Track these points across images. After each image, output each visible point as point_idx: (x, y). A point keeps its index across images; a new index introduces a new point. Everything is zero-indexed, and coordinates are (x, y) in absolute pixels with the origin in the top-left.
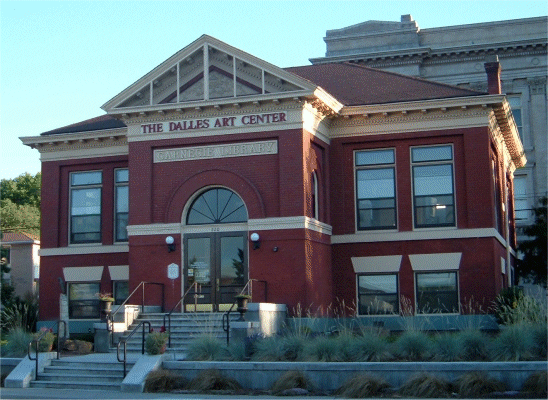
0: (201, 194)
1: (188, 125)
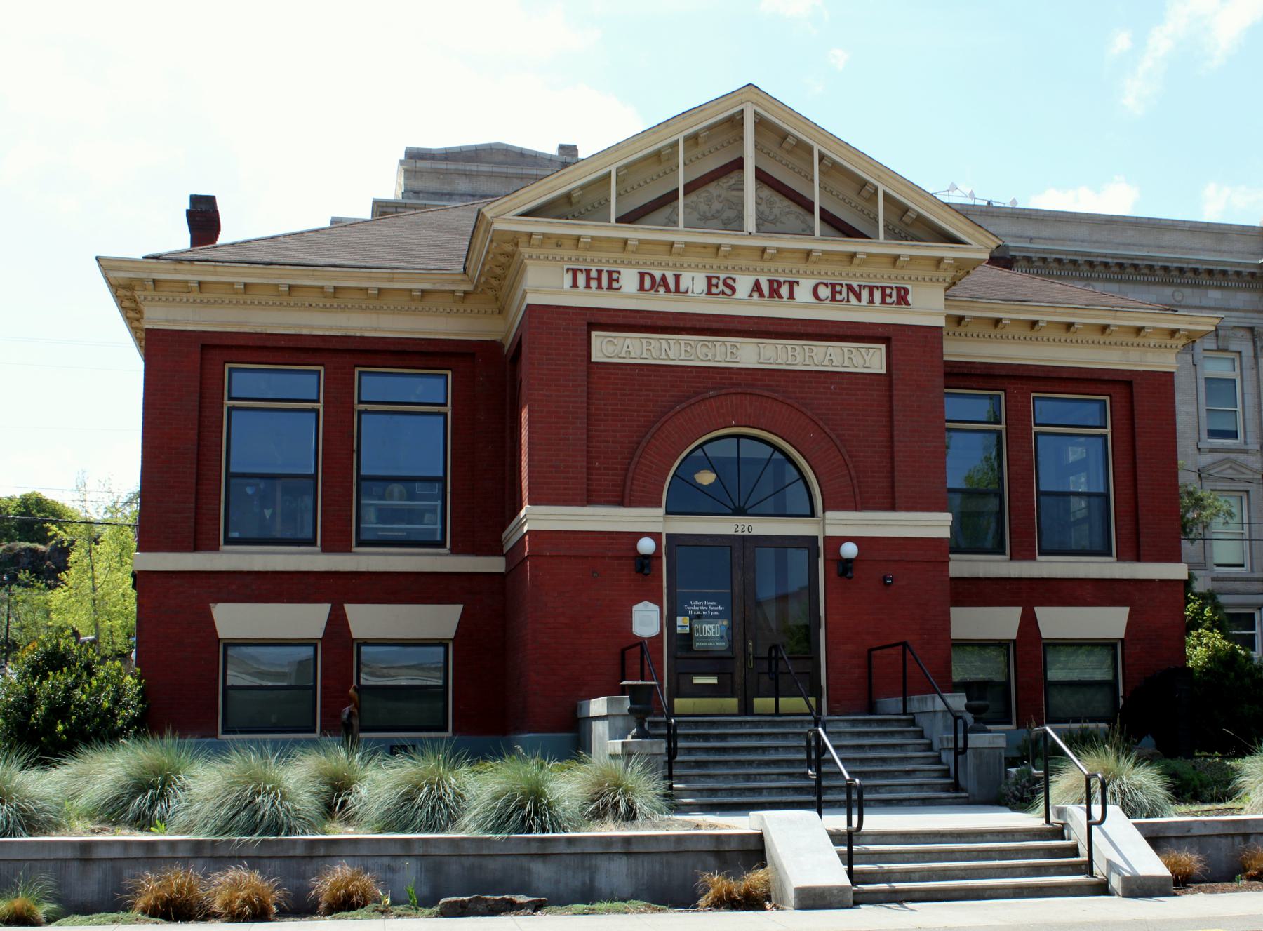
0: (738, 436)
1: (1047, 272)
